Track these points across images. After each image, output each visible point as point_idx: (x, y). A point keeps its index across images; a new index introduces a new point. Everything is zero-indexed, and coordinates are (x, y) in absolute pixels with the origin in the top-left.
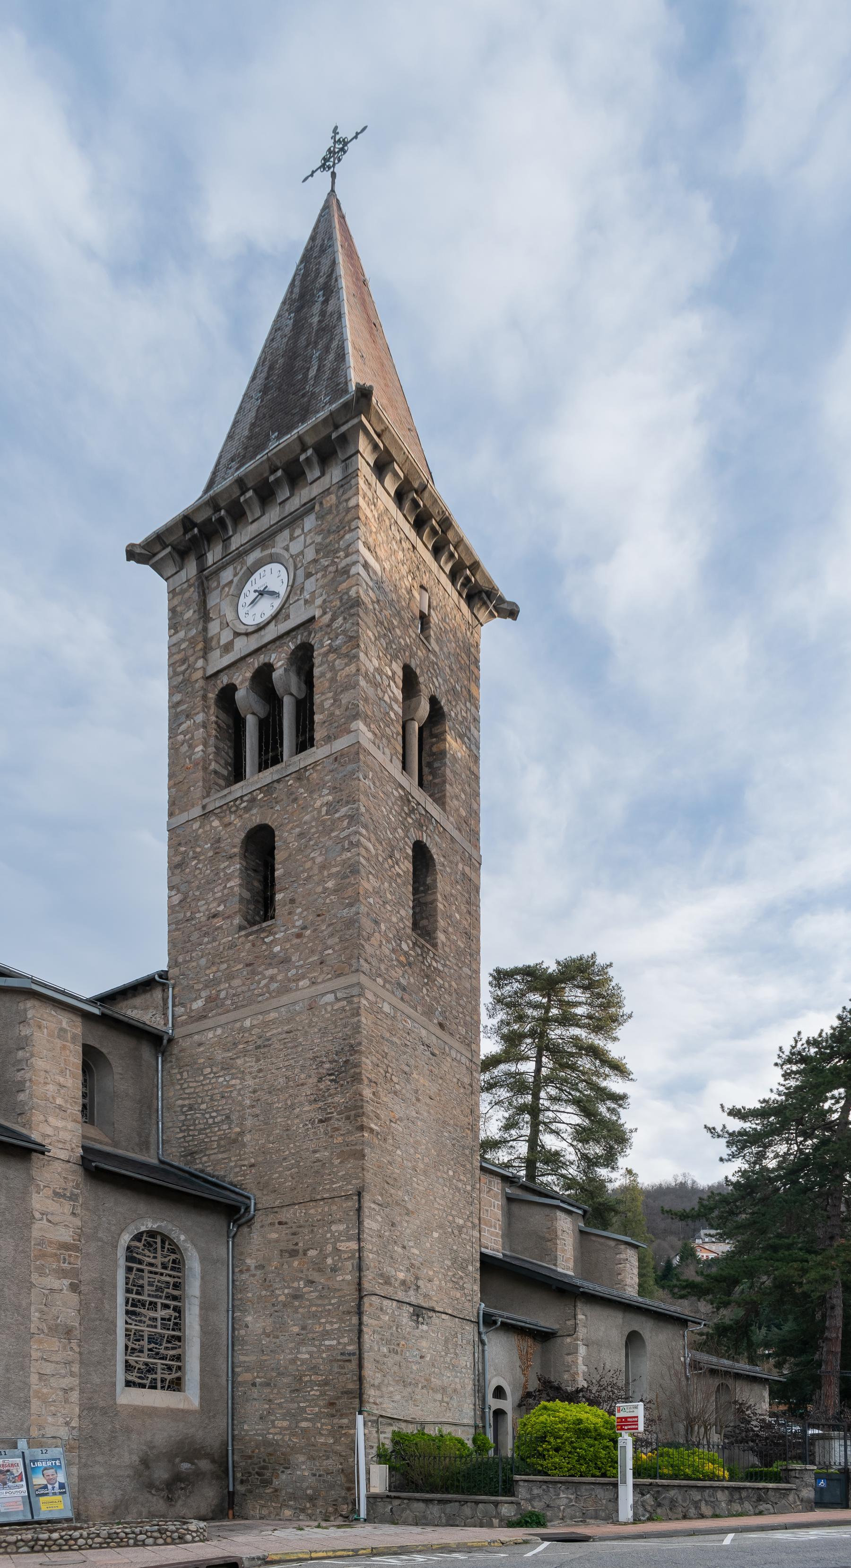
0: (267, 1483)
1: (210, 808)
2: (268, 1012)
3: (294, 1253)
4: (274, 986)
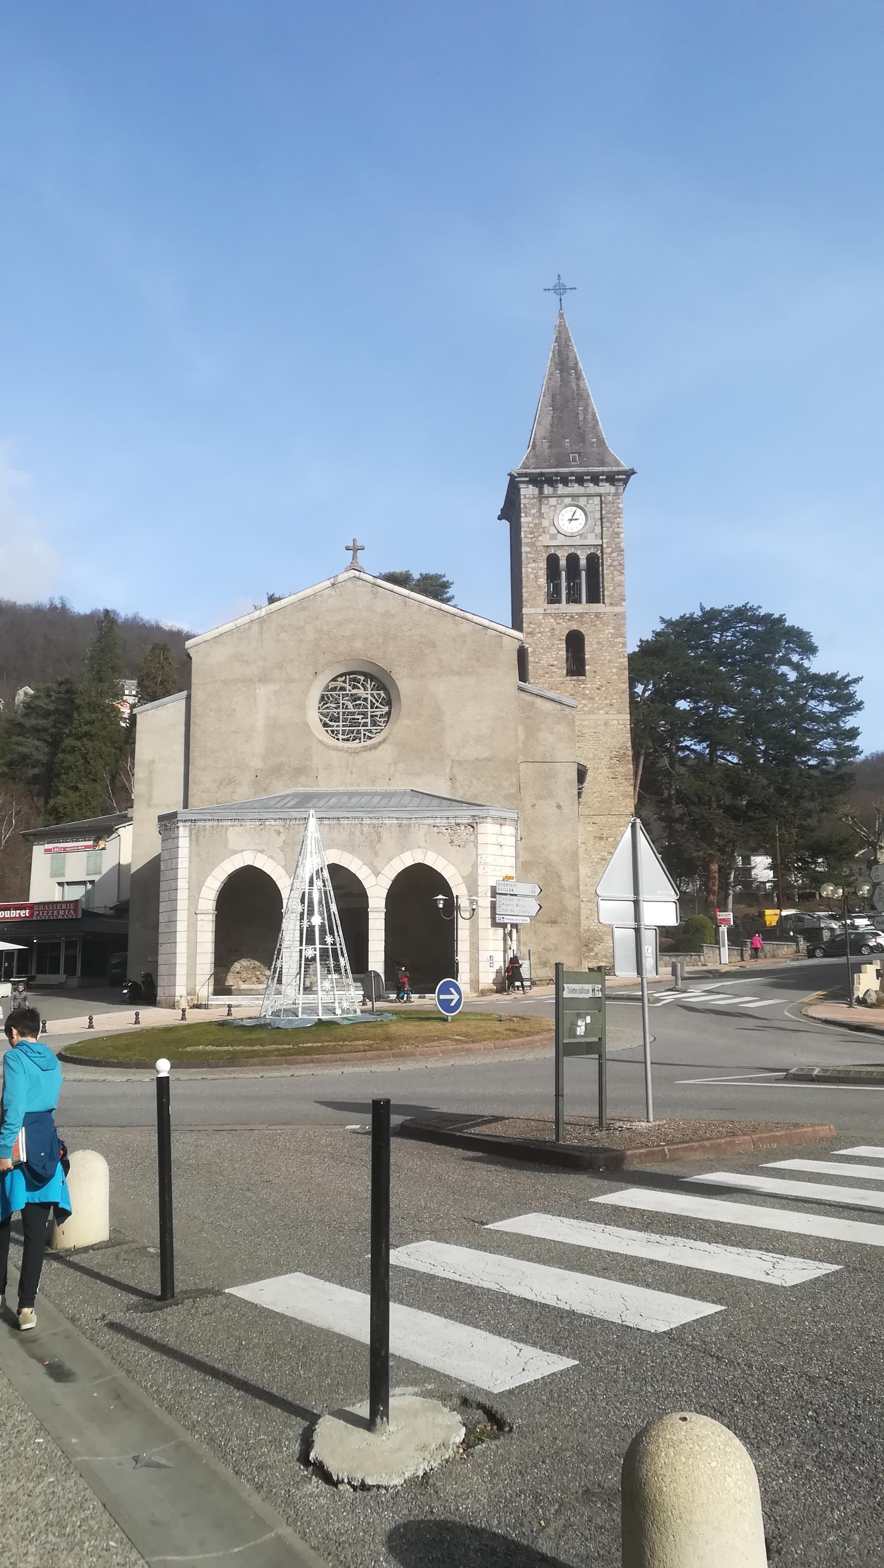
0: (592, 950)
1: (548, 611)
2: (584, 720)
3: (601, 838)
4: (586, 709)
